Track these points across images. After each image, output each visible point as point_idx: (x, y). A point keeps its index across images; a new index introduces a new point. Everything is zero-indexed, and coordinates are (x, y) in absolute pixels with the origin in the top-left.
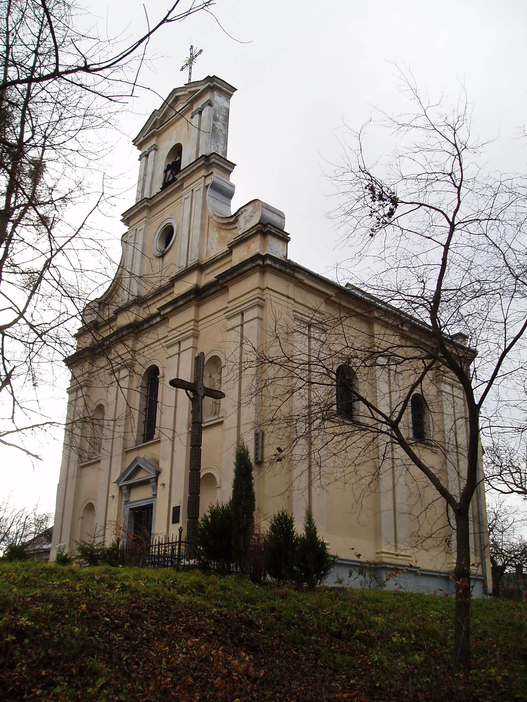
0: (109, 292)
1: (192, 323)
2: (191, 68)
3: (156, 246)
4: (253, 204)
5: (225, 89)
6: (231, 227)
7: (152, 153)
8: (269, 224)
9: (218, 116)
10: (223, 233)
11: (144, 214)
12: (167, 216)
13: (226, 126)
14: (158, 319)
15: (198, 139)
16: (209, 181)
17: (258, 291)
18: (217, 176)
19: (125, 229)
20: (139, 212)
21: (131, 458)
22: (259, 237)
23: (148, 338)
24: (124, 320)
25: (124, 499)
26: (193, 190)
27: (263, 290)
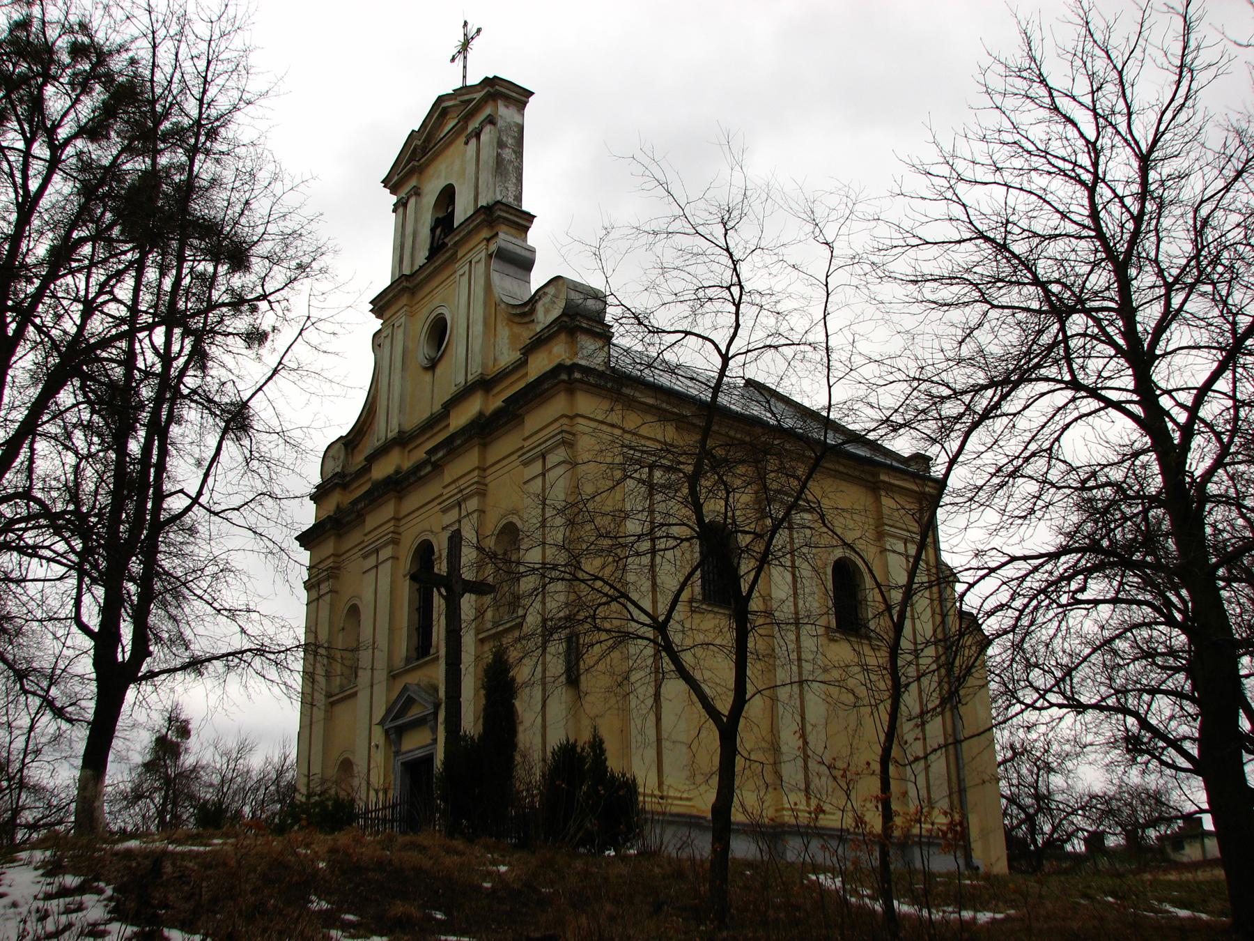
0: (357, 428)
1: (476, 473)
2: (465, 58)
3: (423, 351)
4: (555, 283)
5: (514, 95)
6: (527, 320)
7: (412, 201)
8: (577, 314)
9: (505, 139)
10: (517, 329)
11: (404, 300)
12: (436, 303)
13: (519, 153)
14: (429, 468)
15: (477, 179)
16: (493, 247)
17: (564, 421)
18: (505, 239)
19: (377, 324)
20: (396, 298)
21: (399, 686)
22: (563, 336)
23: (413, 500)
24: (382, 470)
25: (393, 749)
26: (471, 262)
27: (572, 418)
